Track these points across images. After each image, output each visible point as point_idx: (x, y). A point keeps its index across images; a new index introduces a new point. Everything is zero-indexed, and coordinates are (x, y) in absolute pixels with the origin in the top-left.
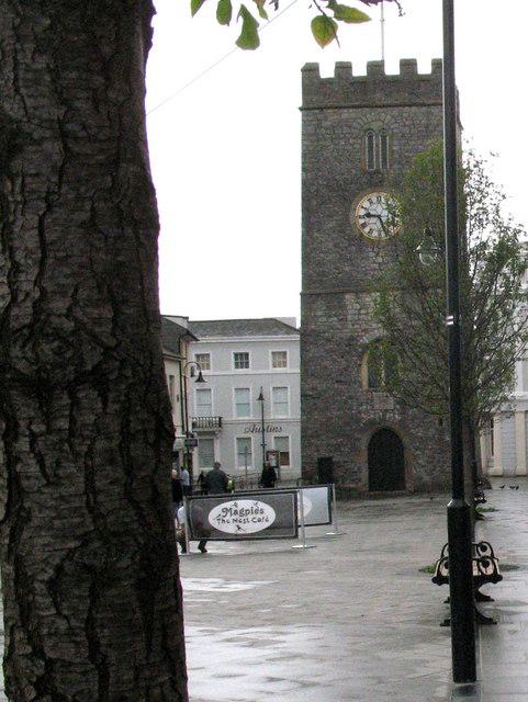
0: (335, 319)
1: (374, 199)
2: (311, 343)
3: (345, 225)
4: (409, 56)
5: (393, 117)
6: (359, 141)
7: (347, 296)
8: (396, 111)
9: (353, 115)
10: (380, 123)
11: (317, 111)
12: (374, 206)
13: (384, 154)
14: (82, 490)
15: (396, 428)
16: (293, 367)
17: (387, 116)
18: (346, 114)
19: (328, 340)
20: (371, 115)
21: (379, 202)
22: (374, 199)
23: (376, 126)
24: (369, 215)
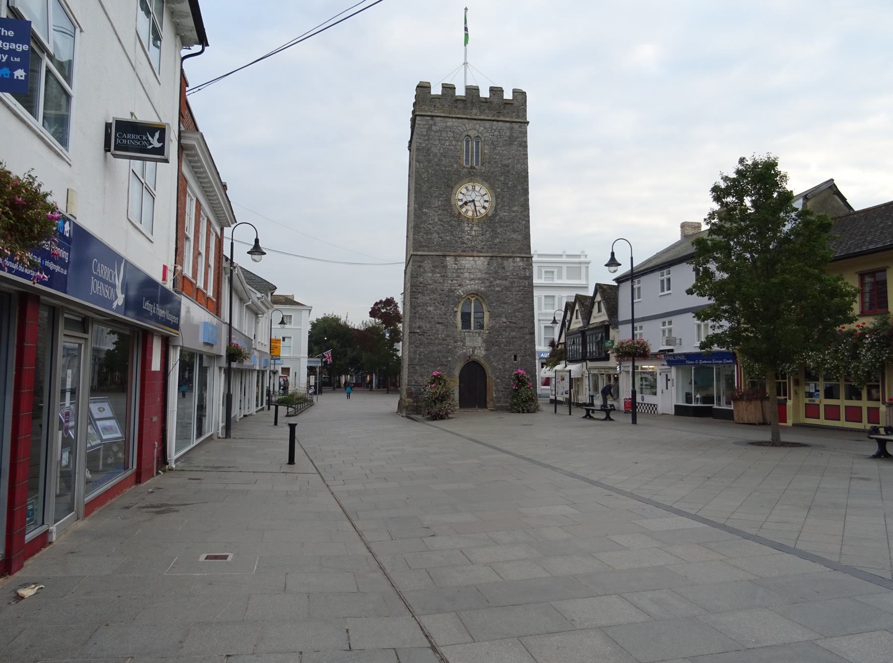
0: (439, 275)
1: (470, 188)
2: (420, 293)
3: (448, 205)
4: (834, 179)
5: (485, 128)
6: (460, 143)
7: (448, 259)
8: (488, 124)
9: (456, 124)
10: (475, 132)
11: (429, 118)
12: (470, 193)
13: (477, 152)
14: (286, 407)
15: (482, 361)
16: (536, 348)
17: (480, 127)
18: (450, 122)
19: (433, 292)
20: (470, 125)
21: (474, 189)
22: (470, 188)
23: (473, 133)
24: (466, 203)
